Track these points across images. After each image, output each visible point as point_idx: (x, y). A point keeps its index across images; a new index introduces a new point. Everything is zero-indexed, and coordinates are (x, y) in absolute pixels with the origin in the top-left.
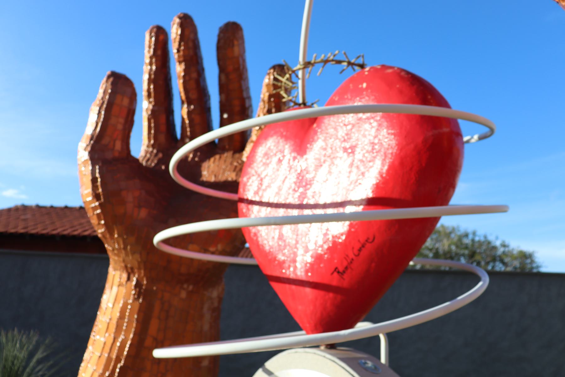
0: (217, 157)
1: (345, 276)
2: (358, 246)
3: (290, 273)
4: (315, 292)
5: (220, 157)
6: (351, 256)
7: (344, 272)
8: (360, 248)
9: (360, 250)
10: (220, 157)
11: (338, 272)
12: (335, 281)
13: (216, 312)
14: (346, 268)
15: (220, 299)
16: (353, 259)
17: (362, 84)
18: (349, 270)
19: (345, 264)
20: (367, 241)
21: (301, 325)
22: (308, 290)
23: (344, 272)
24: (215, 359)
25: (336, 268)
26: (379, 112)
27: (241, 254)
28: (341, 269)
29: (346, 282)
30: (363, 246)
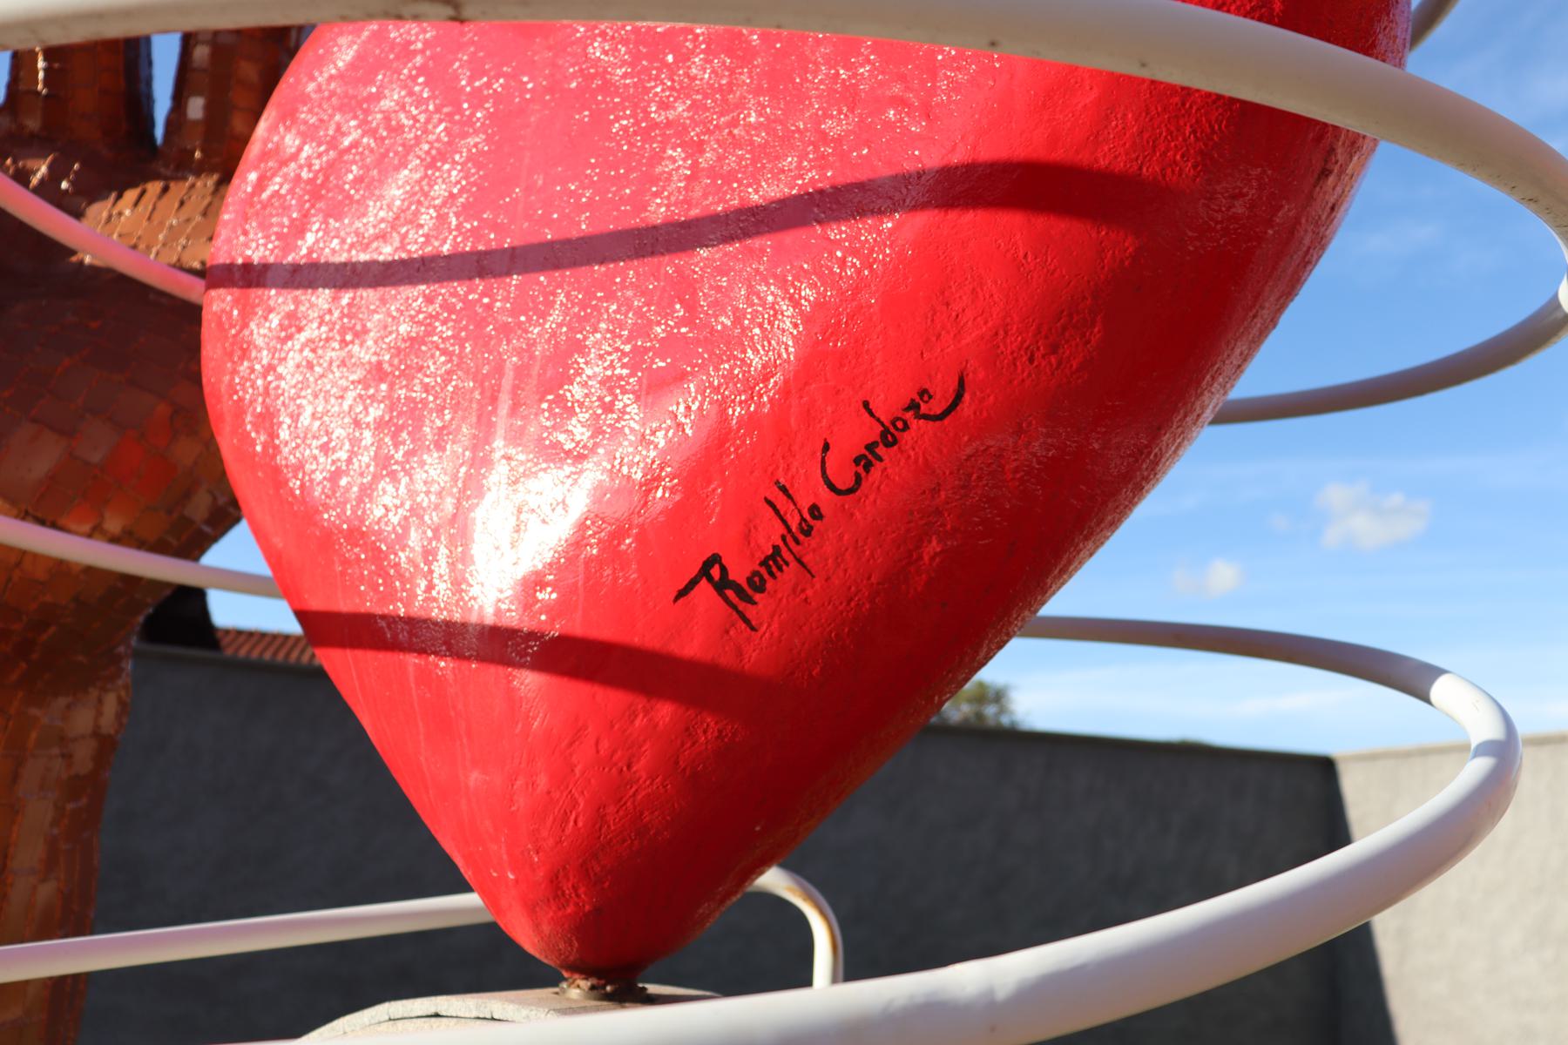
0: (154, 187)
1: (761, 608)
2: (854, 434)
3: (434, 595)
4: (577, 693)
5: (165, 190)
6: (810, 490)
7: (757, 583)
8: (871, 447)
9: (866, 461)
10: (165, 190)
11: (723, 585)
12: (697, 630)
13: (86, 796)
14: (773, 561)
15: (106, 746)
16: (815, 511)
17: (72, 183)
18: (791, 571)
19: (769, 534)
20: (913, 406)
21: (468, 874)
22: (528, 681)
23: (757, 583)
24: (65, 990)
25: (714, 560)
26: (273, 570)
27: (168, 592)
28: (739, 572)
29: (762, 641)
30: (889, 438)
